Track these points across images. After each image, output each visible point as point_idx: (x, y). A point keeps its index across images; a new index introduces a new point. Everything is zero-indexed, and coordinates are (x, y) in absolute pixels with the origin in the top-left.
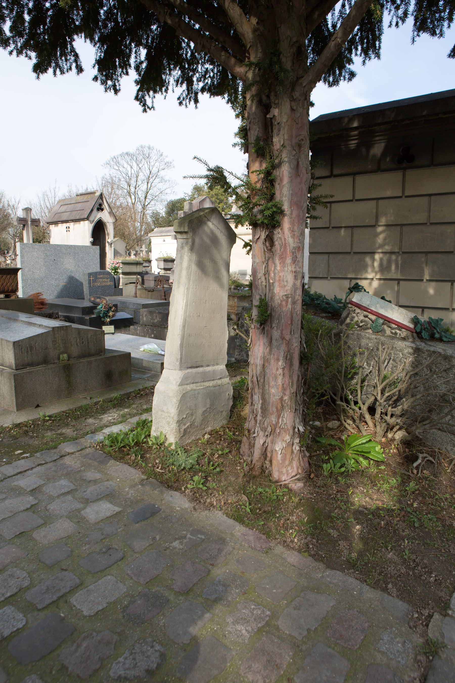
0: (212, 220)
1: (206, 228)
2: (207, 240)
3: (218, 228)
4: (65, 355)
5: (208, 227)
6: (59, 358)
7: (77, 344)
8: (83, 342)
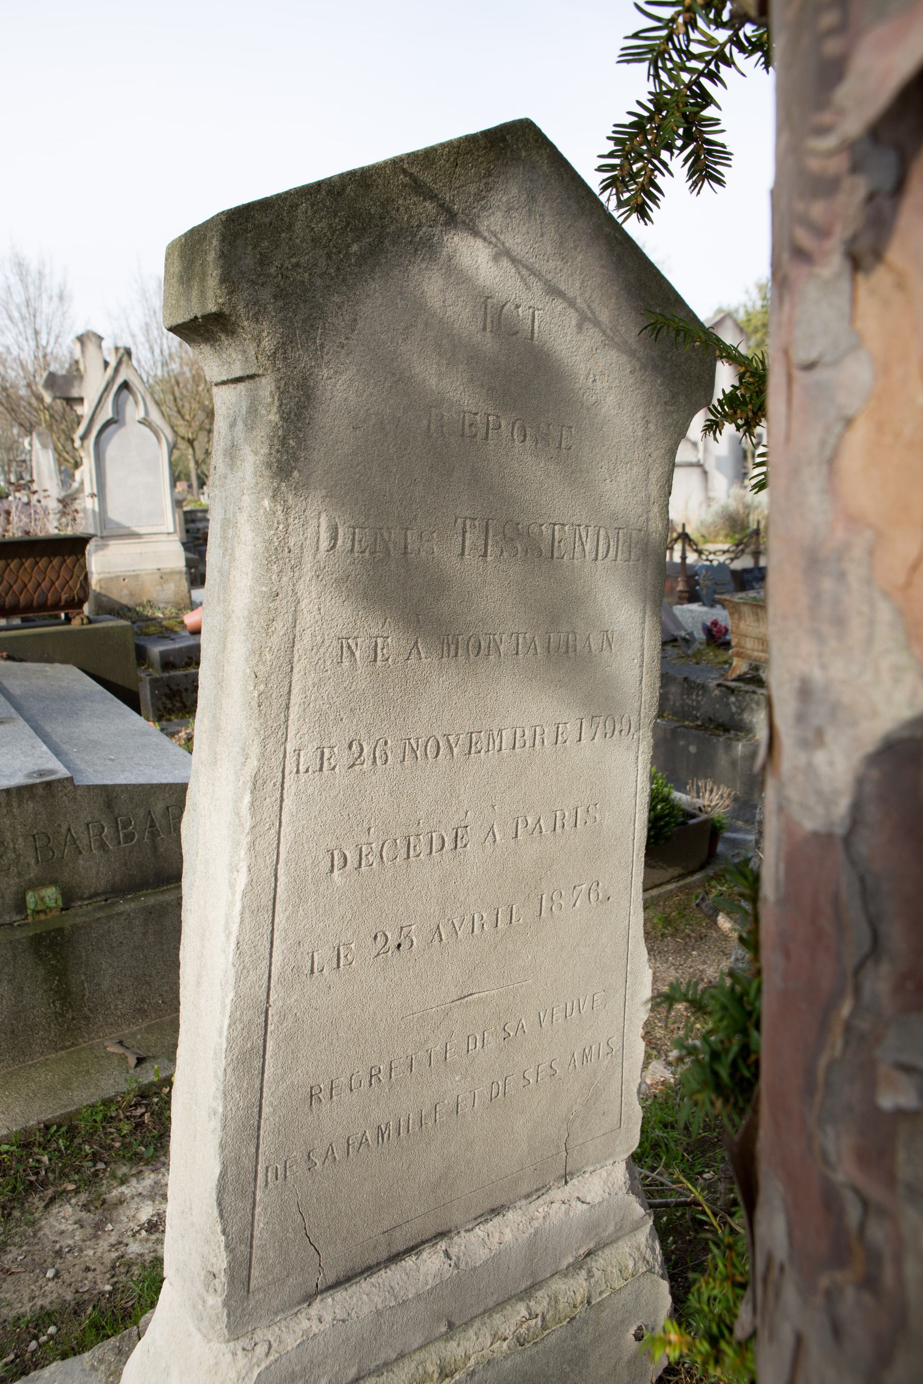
0: (492, 221)
1: (432, 286)
2: (458, 393)
3: (553, 291)
4: (51, 894)
5: (456, 275)
6: (21, 906)
7: (103, 846)
8: (129, 837)
